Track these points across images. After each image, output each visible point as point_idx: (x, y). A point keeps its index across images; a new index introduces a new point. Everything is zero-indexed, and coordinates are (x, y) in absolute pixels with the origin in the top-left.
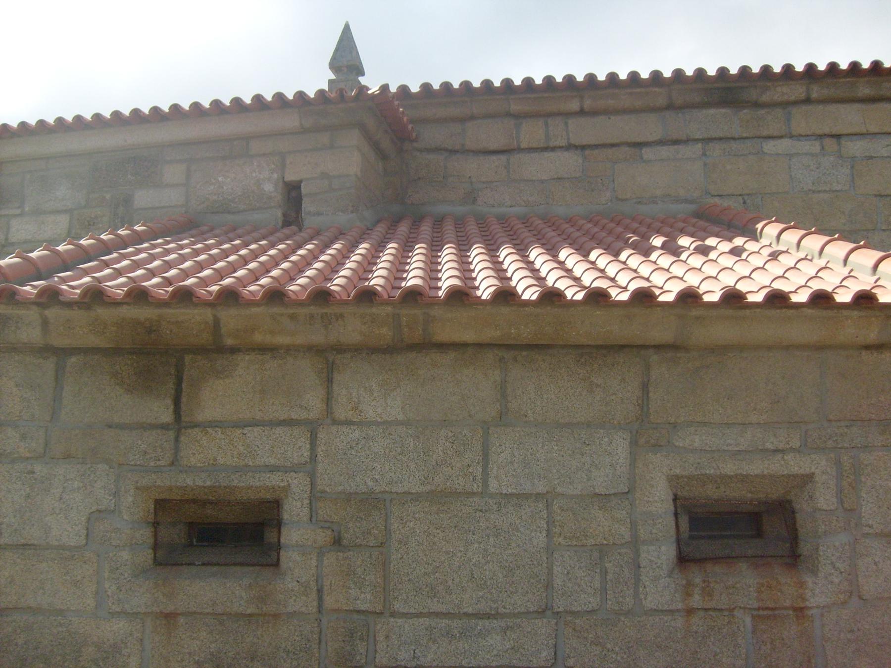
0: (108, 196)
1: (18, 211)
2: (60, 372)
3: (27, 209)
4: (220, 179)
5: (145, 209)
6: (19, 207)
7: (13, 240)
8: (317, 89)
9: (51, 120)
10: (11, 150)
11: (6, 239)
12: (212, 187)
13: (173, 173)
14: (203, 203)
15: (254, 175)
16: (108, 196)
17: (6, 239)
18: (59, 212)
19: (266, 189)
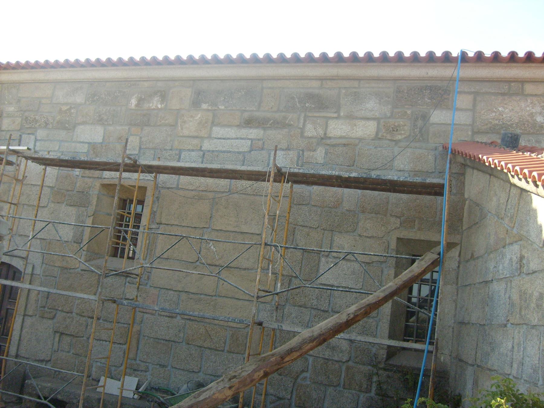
0: (409, 112)
1: (335, 115)
2: (178, 185)
3: (342, 114)
4: (500, 109)
5: (439, 124)
6: (335, 112)
7: (330, 135)
8: (476, 51)
9: (149, 58)
10: (6, 77)
11: (325, 134)
12: (494, 114)
13: (463, 101)
14: (487, 124)
15: (528, 109)
16: (409, 112)
17: (325, 134)
18: (368, 119)
19: (538, 121)
